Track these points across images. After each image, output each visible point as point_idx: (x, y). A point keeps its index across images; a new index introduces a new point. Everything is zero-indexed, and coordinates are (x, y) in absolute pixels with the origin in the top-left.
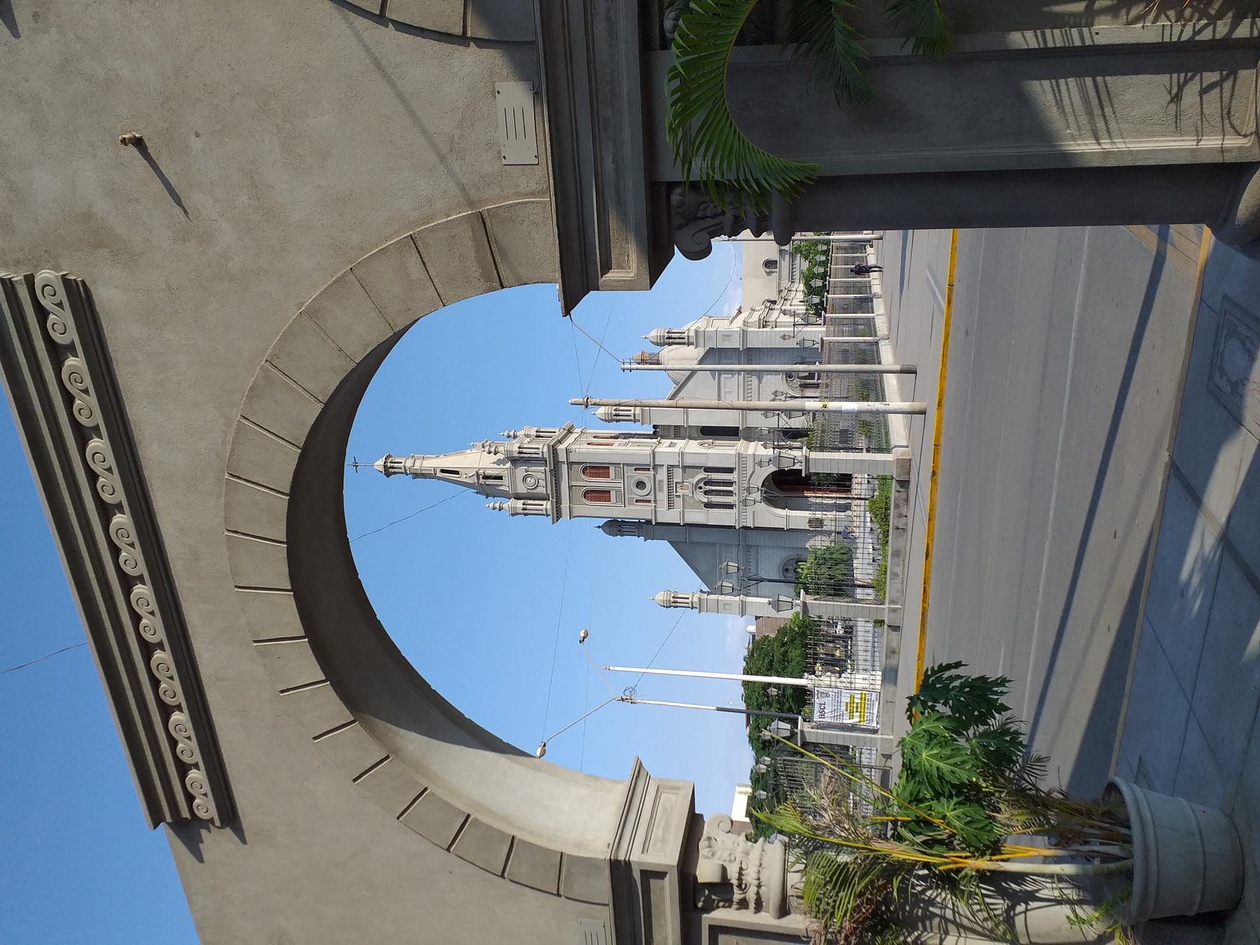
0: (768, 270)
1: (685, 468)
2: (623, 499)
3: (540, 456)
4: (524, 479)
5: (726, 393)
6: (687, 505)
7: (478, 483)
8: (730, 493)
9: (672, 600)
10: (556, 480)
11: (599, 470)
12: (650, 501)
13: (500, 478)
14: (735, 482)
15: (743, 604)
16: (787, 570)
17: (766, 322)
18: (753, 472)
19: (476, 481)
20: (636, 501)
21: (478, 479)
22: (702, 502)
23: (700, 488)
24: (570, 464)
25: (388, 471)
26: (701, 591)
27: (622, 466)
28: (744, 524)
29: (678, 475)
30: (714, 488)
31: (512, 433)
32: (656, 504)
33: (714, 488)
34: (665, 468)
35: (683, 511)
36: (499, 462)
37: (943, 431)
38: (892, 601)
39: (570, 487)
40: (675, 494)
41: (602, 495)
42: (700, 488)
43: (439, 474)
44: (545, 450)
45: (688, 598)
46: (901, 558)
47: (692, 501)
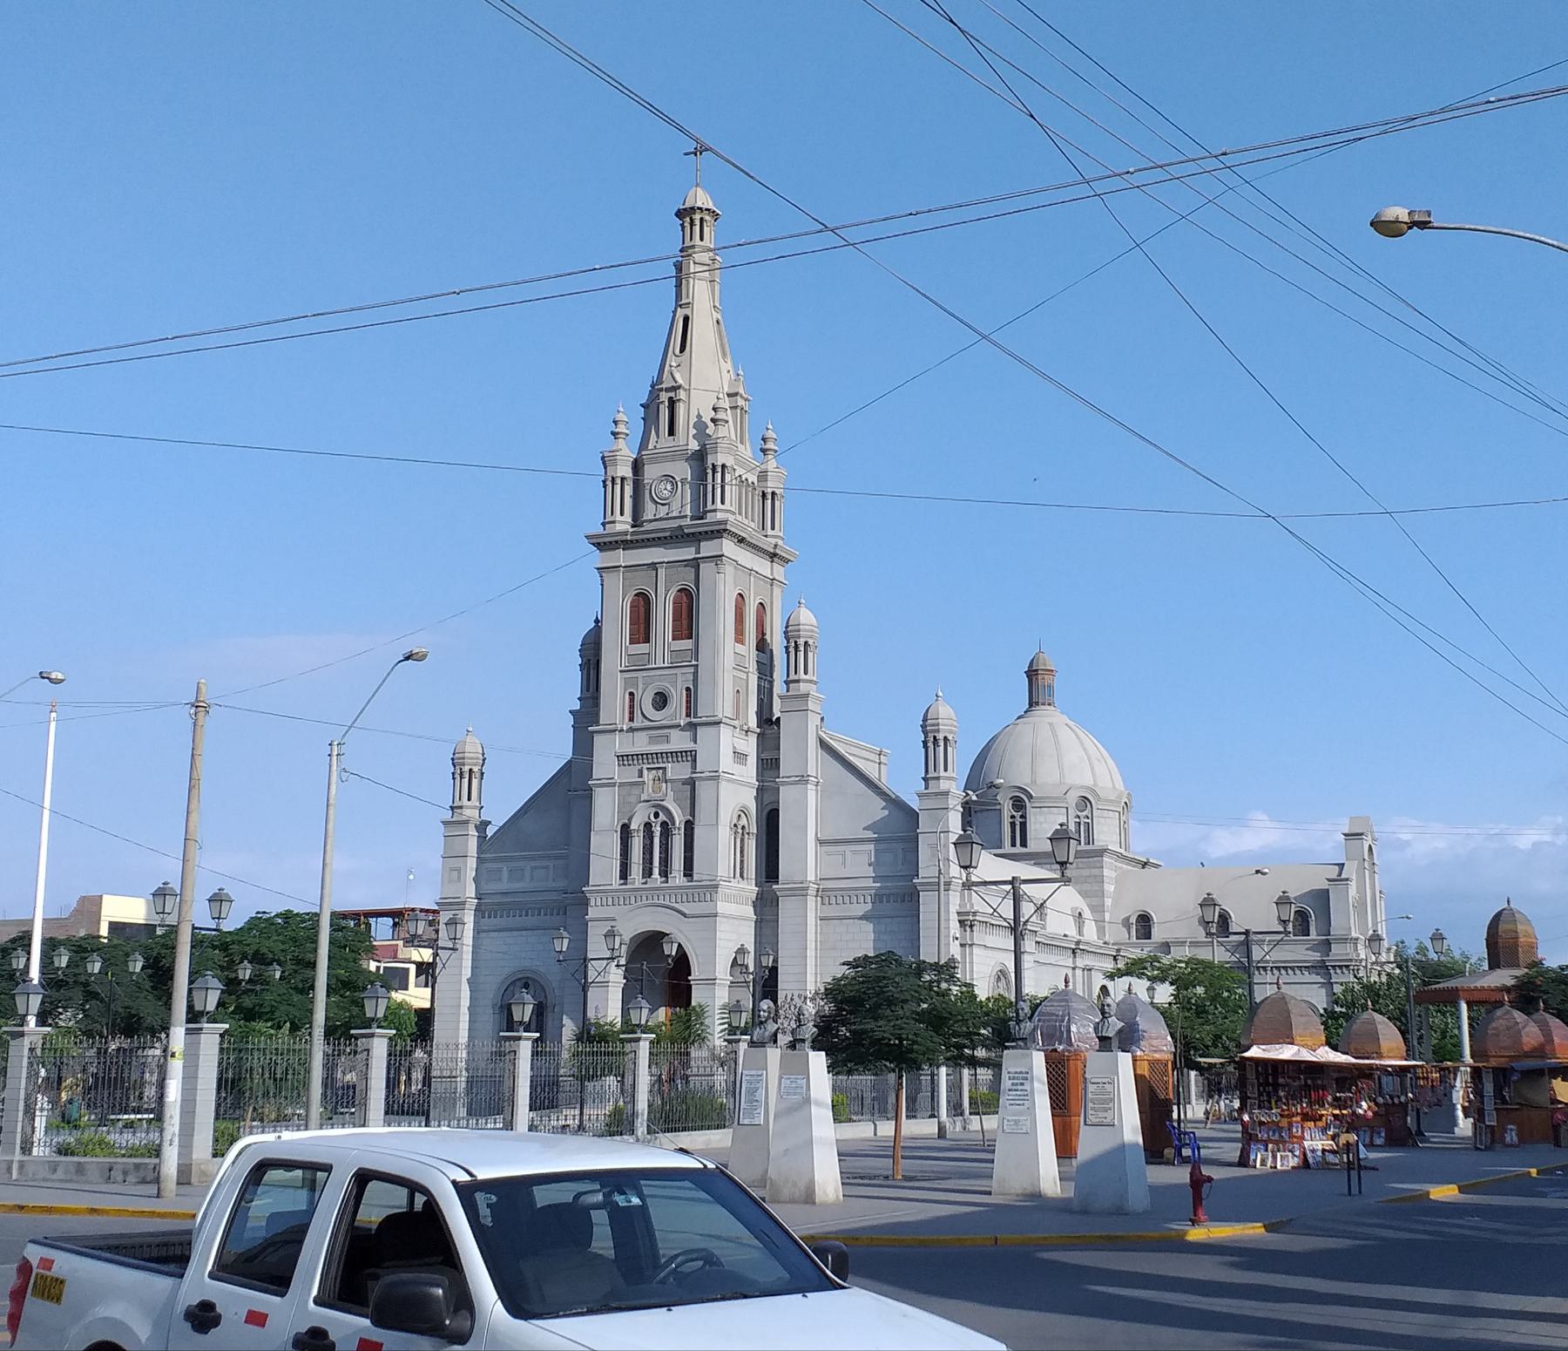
0: (1133, 920)
1: (692, 783)
2: (637, 666)
3: (710, 507)
4: (669, 478)
5: (844, 855)
7: (661, 390)
8: (648, 873)
9: (466, 769)
10: (665, 538)
11: (687, 620)
12: (631, 719)
13: (671, 432)
14: (667, 882)
17: (971, 926)
18: (684, 915)
19: (664, 386)
20: (631, 694)
21: (667, 390)
22: (630, 819)
23: (656, 815)
24: (695, 564)
27: (693, 663)
28: (592, 903)
30: (657, 841)
31: (770, 445)
32: (627, 731)
33: (657, 841)
34: (689, 746)
35: (614, 785)
36: (700, 426)
37: (63, 1217)
38: (23, 1165)
40: (645, 766)
41: (642, 628)
42: (656, 815)
44: (720, 516)
46: (74, 1177)
47: (633, 799)
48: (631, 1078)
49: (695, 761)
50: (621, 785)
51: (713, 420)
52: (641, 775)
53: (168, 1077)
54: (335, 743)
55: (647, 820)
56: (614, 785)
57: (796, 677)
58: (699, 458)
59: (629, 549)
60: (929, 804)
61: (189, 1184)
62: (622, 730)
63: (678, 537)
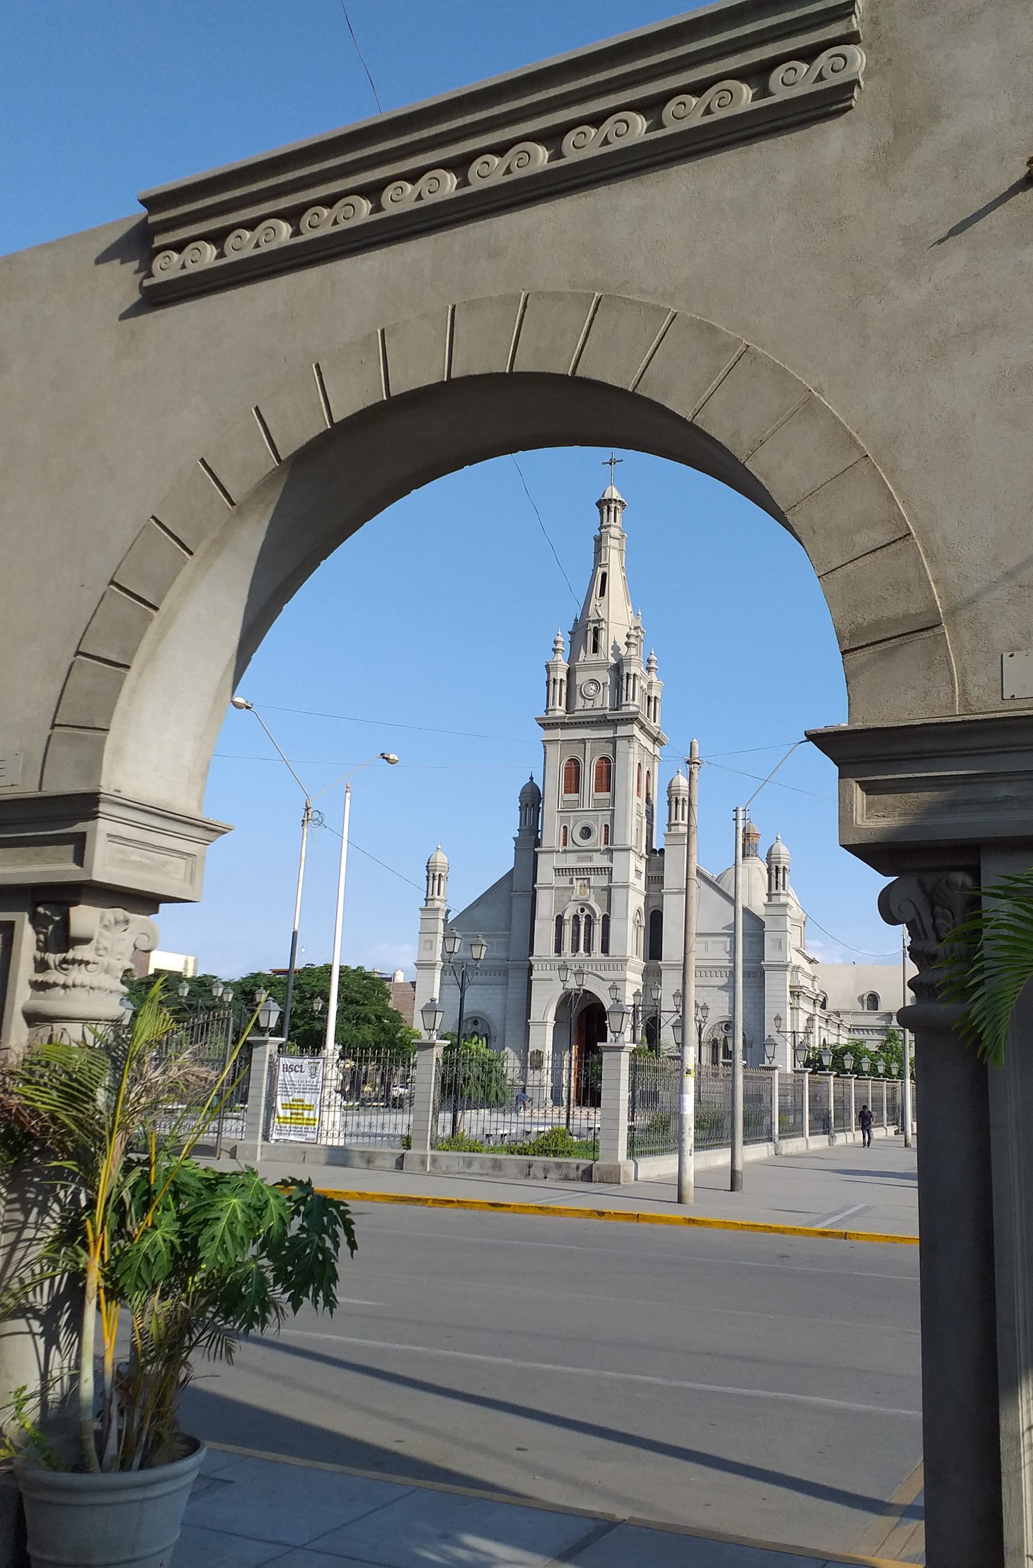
0: (865, 998)
1: (609, 890)
2: (567, 809)
3: (624, 702)
4: (594, 681)
5: (706, 944)
6: (560, 892)
7: (589, 621)
8: (575, 949)
9: (437, 874)
11: (606, 779)
12: (565, 844)
13: (595, 650)
15: (432, 966)
16: (475, 1023)
17: (798, 996)
18: (603, 979)
20: (565, 827)
21: (594, 622)
22: (564, 912)
23: (582, 910)
24: (613, 741)
25: (603, 504)
26: (448, 911)
28: (536, 968)
29: (601, 881)
30: (582, 928)
31: (653, 665)
32: (562, 853)
33: (582, 928)
34: (607, 864)
35: (552, 888)
39: (583, 741)
40: (575, 877)
41: (573, 781)
42: (582, 910)
43: (600, 571)
45: (439, 894)
46: (491, 1172)
47: (565, 899)
48: (769, 1098)
49: (611, 874)
50: (557, 888)
51: (627, 644)
52: (571, 882)
53: (685, 1091)
54: (741, 809)
55: (575, 913)
56: (552, 888)
57: (676, 822)
58: (617, 669)
59: (565, 729)
60: (772, 911)
61: (619, 1183)
62: (558, 852)
63: (602, 722)
